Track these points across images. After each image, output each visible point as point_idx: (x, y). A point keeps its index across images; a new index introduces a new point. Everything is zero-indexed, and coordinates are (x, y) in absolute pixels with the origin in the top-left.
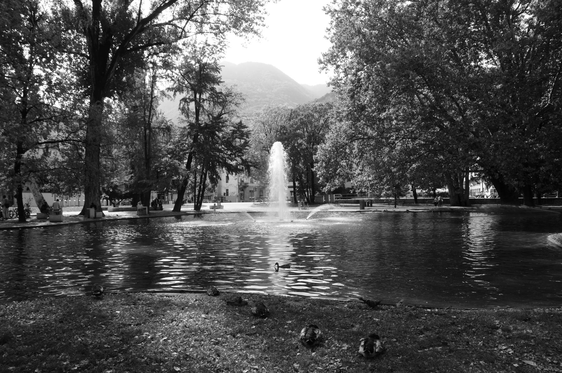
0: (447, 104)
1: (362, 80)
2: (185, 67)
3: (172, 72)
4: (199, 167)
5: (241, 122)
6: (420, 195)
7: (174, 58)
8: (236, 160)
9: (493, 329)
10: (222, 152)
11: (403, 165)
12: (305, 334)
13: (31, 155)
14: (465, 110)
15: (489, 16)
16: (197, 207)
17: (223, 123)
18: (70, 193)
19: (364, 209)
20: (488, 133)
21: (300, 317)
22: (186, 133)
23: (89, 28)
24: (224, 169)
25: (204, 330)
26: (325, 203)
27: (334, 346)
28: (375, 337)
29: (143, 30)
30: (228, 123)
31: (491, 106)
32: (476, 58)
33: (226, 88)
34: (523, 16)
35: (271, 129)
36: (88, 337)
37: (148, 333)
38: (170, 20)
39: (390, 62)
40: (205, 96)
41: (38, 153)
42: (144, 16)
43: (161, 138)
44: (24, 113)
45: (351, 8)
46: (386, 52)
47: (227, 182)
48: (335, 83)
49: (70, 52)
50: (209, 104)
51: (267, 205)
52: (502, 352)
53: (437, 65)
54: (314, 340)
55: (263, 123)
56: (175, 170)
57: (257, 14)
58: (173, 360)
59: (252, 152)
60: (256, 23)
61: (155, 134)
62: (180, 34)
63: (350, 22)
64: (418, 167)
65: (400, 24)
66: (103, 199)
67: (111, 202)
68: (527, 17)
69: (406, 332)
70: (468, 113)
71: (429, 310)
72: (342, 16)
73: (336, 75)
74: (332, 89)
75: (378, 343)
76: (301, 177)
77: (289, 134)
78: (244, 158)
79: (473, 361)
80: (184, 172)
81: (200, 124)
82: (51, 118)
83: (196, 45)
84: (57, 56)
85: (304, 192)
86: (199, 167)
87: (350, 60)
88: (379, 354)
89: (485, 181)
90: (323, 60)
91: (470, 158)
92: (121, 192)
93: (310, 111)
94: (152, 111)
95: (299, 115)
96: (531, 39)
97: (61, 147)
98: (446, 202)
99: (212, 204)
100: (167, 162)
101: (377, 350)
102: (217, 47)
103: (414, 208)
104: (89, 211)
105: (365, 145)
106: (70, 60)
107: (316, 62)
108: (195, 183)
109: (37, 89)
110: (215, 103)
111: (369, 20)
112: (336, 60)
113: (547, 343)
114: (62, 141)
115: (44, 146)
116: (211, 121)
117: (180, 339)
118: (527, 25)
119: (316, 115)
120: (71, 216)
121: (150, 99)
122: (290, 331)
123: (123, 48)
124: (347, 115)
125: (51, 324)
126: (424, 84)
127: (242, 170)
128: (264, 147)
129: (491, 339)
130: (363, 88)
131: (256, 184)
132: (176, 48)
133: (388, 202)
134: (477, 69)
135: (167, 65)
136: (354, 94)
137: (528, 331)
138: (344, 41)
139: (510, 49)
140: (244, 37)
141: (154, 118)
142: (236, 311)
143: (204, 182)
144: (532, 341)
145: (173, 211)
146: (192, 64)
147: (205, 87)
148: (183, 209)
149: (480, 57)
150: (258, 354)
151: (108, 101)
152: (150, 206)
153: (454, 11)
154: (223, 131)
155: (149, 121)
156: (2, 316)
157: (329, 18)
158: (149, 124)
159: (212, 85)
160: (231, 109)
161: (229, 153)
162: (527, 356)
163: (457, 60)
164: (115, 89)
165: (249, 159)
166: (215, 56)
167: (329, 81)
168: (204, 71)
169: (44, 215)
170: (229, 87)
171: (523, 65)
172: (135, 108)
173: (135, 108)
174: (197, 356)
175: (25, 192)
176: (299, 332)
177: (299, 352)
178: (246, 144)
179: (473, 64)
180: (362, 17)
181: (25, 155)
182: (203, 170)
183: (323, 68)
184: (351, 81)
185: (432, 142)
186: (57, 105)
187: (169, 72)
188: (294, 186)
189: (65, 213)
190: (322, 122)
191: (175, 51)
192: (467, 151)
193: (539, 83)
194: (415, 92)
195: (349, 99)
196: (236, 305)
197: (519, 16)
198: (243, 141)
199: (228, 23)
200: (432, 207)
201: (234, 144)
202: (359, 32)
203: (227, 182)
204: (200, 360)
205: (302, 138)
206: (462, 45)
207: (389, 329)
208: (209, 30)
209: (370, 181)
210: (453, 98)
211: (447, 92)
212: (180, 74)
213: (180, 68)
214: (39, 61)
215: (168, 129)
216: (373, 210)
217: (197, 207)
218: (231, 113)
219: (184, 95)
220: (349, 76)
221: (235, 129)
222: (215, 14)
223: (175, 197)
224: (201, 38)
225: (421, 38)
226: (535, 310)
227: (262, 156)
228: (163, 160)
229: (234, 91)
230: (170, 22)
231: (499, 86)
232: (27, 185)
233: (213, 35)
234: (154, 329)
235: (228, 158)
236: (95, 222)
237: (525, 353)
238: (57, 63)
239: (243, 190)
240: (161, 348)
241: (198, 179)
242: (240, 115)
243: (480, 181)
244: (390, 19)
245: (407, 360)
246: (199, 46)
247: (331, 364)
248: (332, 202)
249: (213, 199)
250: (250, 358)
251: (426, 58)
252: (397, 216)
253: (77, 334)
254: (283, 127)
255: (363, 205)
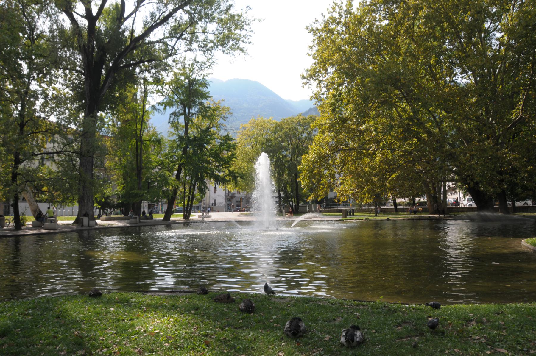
0: (424, 116)
1: (343, 94)
2: (175, 82)
3: (163, 88)
4: (188, 178)
5: (228, 135)
6: (400, 205)
7: (163, 73)
8: (224, 172)
9: (467, 321)
10: (210, 163)
11: (383, 175)
12: (290, 326)
13: (28, 166)
14: (442, 122)
15: (462, 34)
16: (186, 217)
17: (211, 136)
18: (63, 202)
19: (346, 217)
20: (464, 144)
21: (285, 312)
22: (175, 145)
23: (84, 45)
24: (212, 180)
25: (193, 324)
26: (309, 212)
27: (317, 337)
28: (356, 328)
29: (135, 48)
30: (216, 136)
31: (467, 118)
32: (451, 74)
33: (215, 103)
34: (494, 35)
35: (257, 142)
36: (84, 330)
37: (140, 327)
38: (161, 38)
39: (369, 77)
40: (194, 110)
41: (34, 164)
42: (136, 35)
43: (151, 149)
44: (22, 125)
45: (333, 26)
46: (366, 68)
47: (215, 192)
48: (317, 97)
49: (65, 69)
50: (198, 117)
51: (252, 215)
52: (475, 341)
53: (414, 80)
54: (298, 332)
55: (249, 136)
56: (165, 181)
57: (243, 32)
58: (164, 350)
59: (238, 164)
60: (243, 41)
61: (147, 147)
62: (170, 52)
63: (331, 39)
64: (398, 177)
65: (378, 42)
66: (96, 209)
67: (103, 211)
68: (498, 35)
69: (384, 324)
70: (445, 124)
71: (407, 306)
72: (324, 35)
73: (318, 89)
74: (315, 103)
75: (358, 333)
76: (286, 187)
77: (274, 147)
78: (231, 169)
79: (448, 349)
80: (173, 183)
81: (189, 137)
82: (46, 131)
83: (186, 62)
84: (53, 72)
85: (289, 202)
86: (188, 178)
87: (331, 76)
88: (359, 344)
89: (462, 190)
90: (305, 76)
91: (446, 167)
92: (114, 202)
93: (294, 125)
94: (144, 124)
95: (284, 128)
96: (502, 56)
97: (56, 157)
98: (424, 211)
99: (201, 214)
100: (157, 173)
101: (357, 340)
102: (205, 64)
103: (394, 216)
104: (82, 219)
105: (347, 156)
106: (66, 75)
107: (299, 77)
108: (185, 193)
109: (34, 104)
110: (204, 117)
111: (349, 38)
112: (318, 75)
113: (518, 333)
114: (57, 153)
115: (39, 157)
116: (200, 134)
117: (171, 331)
118: (498, 43)
119: (300, 129)
120: (64, 225)
121: (141, 113)
122: (275, 325)
123: (116, 64)
124: (329, 127)
125: (48, 319)
126: (402, 98)
127: (229, 181)
128: (250, 159)
129: (466, 330)
130: (345, 102)
131: (243, 194)
132: (166, 64)
133: (370, 211)
134: (452, 84)
135: (158, 81)
136: (335, 107)
137: (501, 322)
138: (325, 58)
139: (483, 65)
140: (231, 54)
141: (146, 131)
142: (225, 307)
143: (193, 193)
144: (504, 331)
145: (163, 220)
146: (181, 80)
147: (194, 102)
148: (172, 218)
149: (455, 73)
150: (245, 345)
151: (101, 115)
152: (141, 216)
153: (429, 29)
154: (211, 143)
155: (140, 134)
156: (2, 312)
157: (311, 36)
158: (141, 137)
159: (201, 100)
160: (219, 122)
161: (217, 164)
162: (498, 345)
163: (434, 76)
164: (108, 104)
165: (236, 170)
166: (204, 72)
167: (311, 95)
168: (193, 87)
169: (39, 223)
170: (217, 102)
171: (495, 79)
172: (125, 122)
173: (125, 122)
174: (187, 346)
175: (21, 202)
176: (284, 325)
177: (284, 342)
178: (233, 156)
179: (448, 79)
180: (342, 36)
181: (21, 166)
182: (192, 181)
183: (306, 83)
184: (333, 95)
185: (410, 153)
186: (53, 119)
187: (160, 87)
188: (279, 197)
189: (60, 222)
190: (305, 134)
191: (167, 67)
192: (443, 161)
193: (512, 97)
194: (394, 105)
195: (330, 112)
196: (224, 302)
197: (491, 35)
198: (230, 153)
199: (215, 41)
200: (412, 216)
201: (221, 156)
202: (339, 49)
203: (215, 192)
204: (191, 350)
205: (287, 151)
206: (438, 62)
207: (369, 322)
208: (198, 48)
209: (352, 190)
210: (430, 111)
211: (424, 106)
212: (170, 90)
213: (170, 84)
214: (36, 77)
215: (159, 142)
216: (355, 218)
217: (186, 217)
218: (218, 126)
219: (174, 109)
220: (331, 91)
221: (223, 142)
222: (204, 32)
223: (165, 207)
224: (190, 56)
225: (400, 55)
226: (508, 305)
227: (248, 168)
228: (154, 171)
229: (222, 105)
230: (161, 40)
231: (474, 100)
232: (23, 195)
233: (202, 53)
234: (147, 323)
235: (216, 169)
236: (88, 230)
237: (497, 342)
238: (54, 78)
239: (230, 200)
240: (153, 340)
241: (187, 190)
242: (228, 129)
243: (457, 190)
244: (369, 37)
245: (385, 349)
246: (188, 63)
247: (314, 352)
248: (315, 211)
249: (202, 209)
250: (238, 347)
251: (403, 74)
252: (377, 225)
253: (73, 328)
254: (269, 140)
255: (346, 214)
